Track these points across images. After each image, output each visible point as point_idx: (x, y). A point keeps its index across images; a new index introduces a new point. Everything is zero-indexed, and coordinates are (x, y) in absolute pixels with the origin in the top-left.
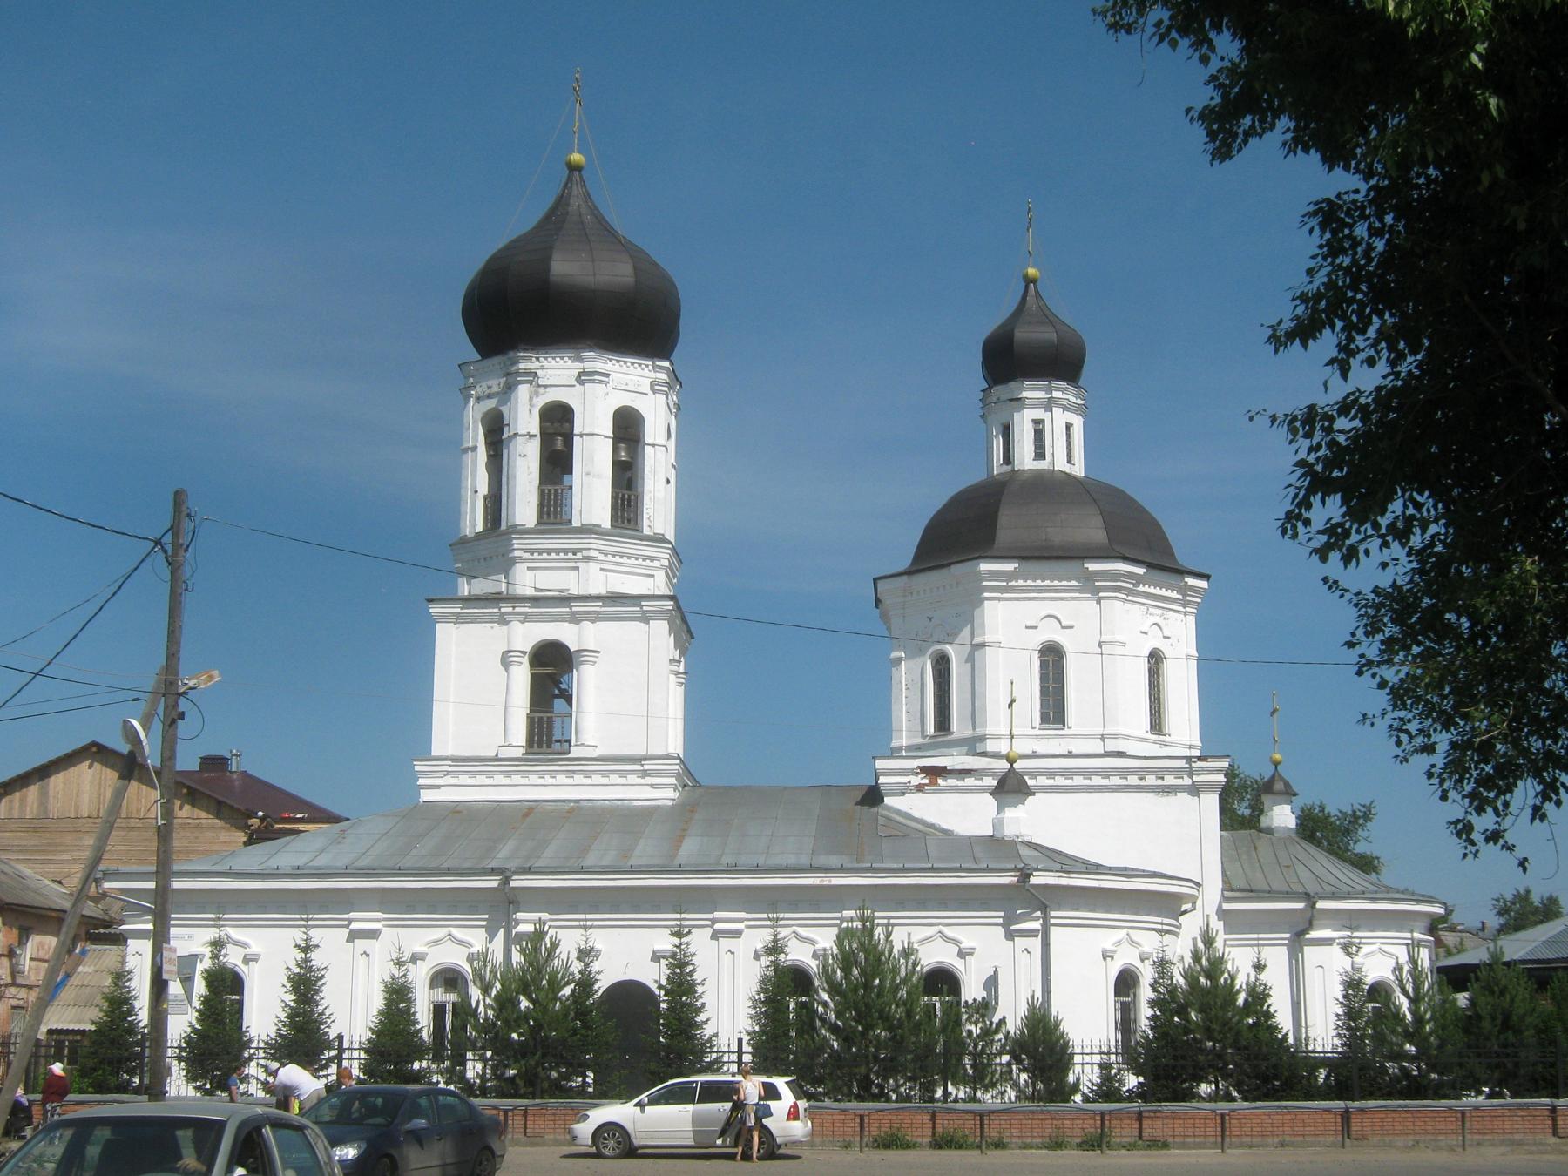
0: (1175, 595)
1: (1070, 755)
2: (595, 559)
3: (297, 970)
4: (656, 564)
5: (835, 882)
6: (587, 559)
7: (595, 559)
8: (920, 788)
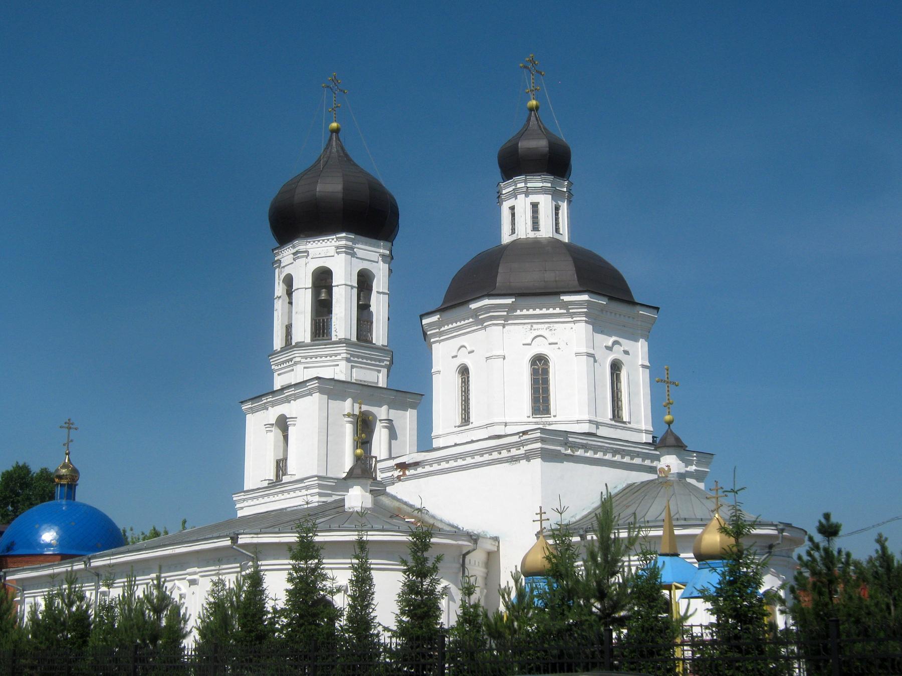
0: (558, 311)
1: (472, 442)
2: (299, 362)
3: (719, 586)
4: (339, 357)
5: (113, 561)
6: (296, 363)
7: (299, 362)
8: (399, 478)
